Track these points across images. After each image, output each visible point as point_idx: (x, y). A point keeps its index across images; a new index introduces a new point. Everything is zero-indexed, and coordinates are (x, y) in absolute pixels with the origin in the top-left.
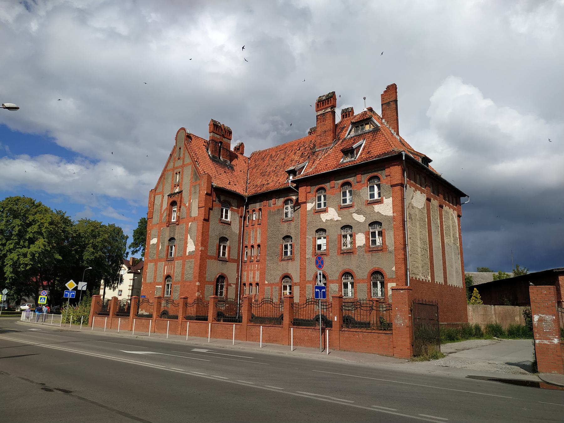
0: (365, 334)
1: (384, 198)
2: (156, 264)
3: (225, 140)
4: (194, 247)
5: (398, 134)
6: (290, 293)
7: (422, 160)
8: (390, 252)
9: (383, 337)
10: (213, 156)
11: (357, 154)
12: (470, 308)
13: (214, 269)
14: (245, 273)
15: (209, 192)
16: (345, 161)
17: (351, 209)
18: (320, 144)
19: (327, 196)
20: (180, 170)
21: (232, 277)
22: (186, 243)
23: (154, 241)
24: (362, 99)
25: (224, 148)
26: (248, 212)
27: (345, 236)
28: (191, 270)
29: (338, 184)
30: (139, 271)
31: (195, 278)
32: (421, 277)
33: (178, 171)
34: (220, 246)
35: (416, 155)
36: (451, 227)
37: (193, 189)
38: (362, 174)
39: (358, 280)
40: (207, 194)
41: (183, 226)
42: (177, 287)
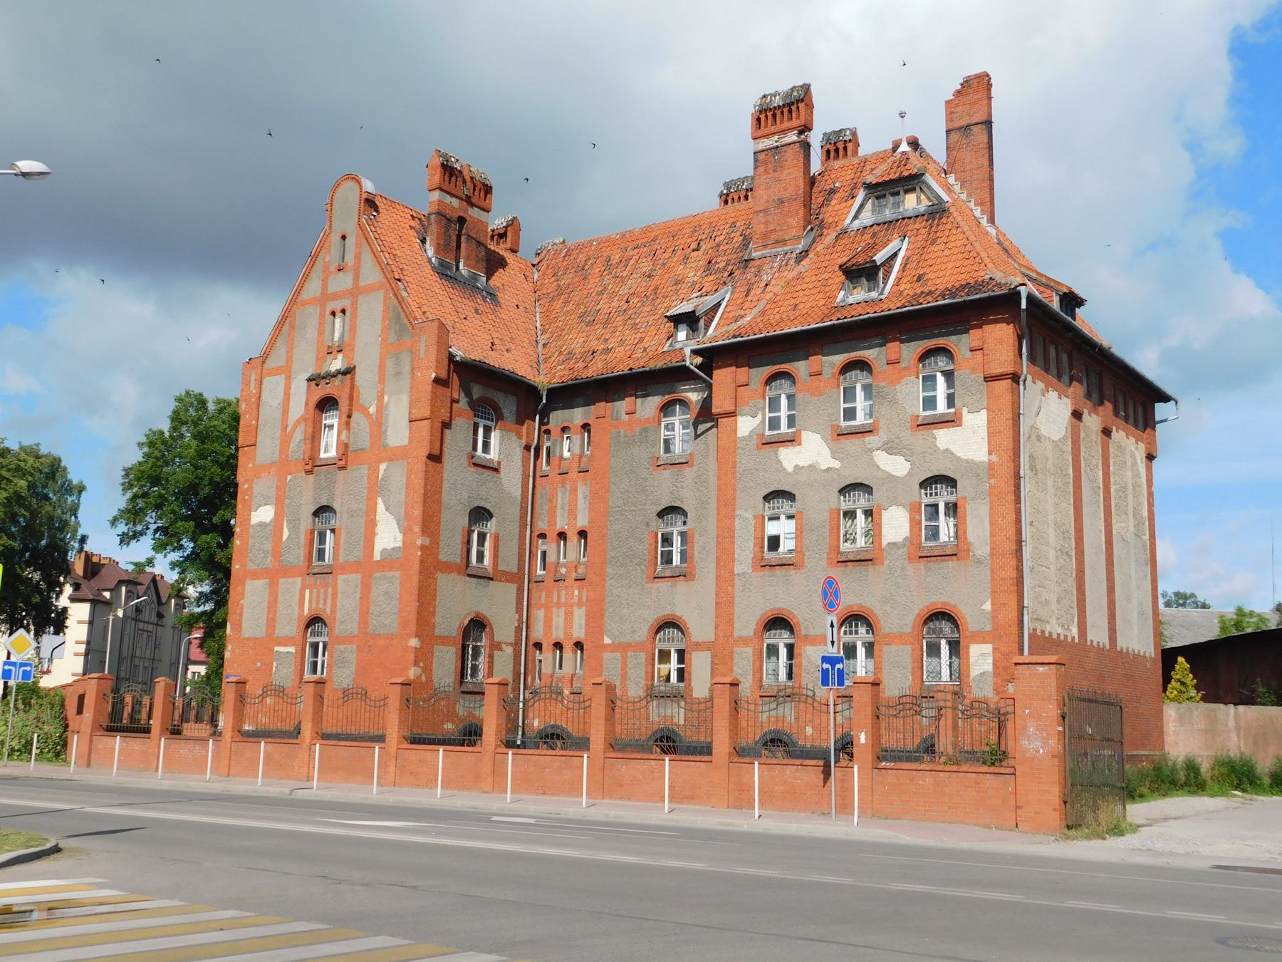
0: (942, 774)
1: (965, 411)
2: (273, 585)
3: (474, 213)
4: (400, 536)
5: (992, 220)
6: (681, 674)
7: (1061, 301)
8: (979, 562)
9: (990, 781)
10: (442, 264)
11: (885, 283)
12: (1171, 711)
13: (457, 601)
14: (539, 614)
15: (444, 375)
16: (851, 300)
17: (869, 439)
18: (765, 236)
19: (800, 397)
20: (346, 303)
21: (503, 626)
22: (371, 525)
23: (263, 514)
24: (880, 107)
25: (469, 237)
26: (548, 432)
27: (850, 514)
28: (390, 604)
29: (831, 364)
30: (107, 595)
31: (404, 624)
32: (1054, 629)
33: (337, 306)
34: (470, 532)
35: (1047, 286)
36: (1130, 487)
37: (389, 363)
38: (902, 342)
39: (887, 635)
40: (437, 381)
41: (358, 473)
42: (349, 652)
